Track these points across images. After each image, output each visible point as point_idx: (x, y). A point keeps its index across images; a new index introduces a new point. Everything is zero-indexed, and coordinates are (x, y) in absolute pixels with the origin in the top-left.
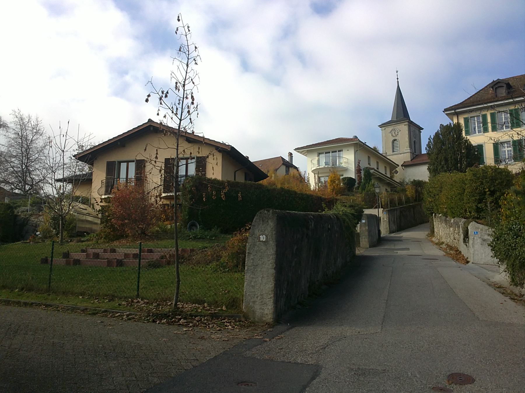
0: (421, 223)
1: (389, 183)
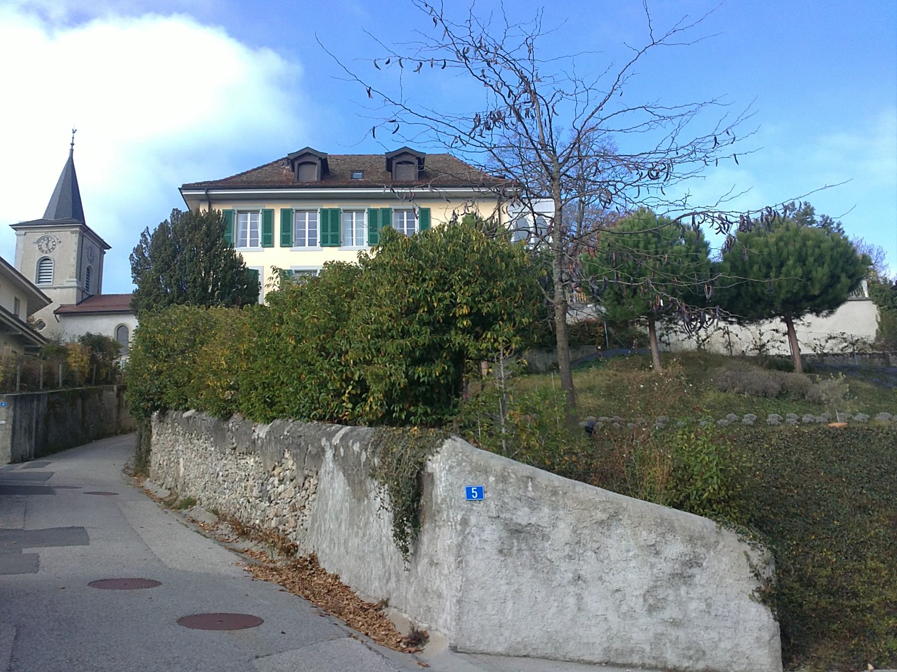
0: (99, 437)
1: (22, 335)
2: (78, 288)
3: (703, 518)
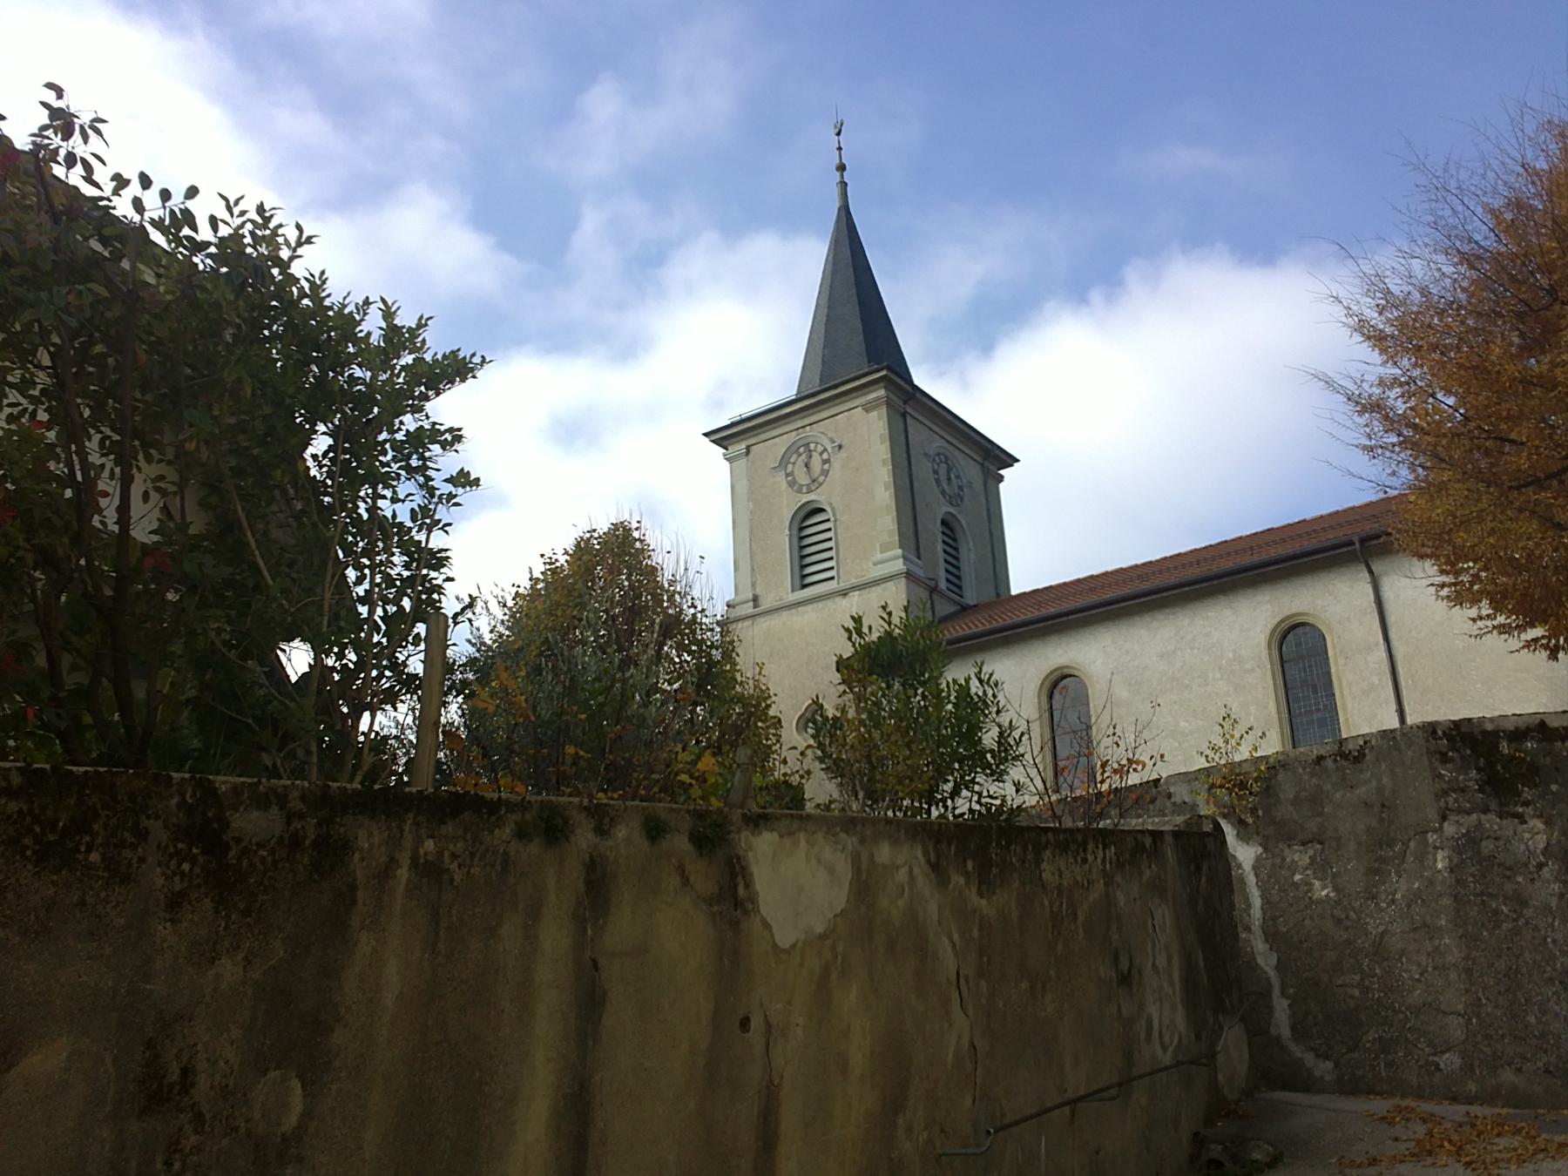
2: (909, 575)
3: (1496, 714)
